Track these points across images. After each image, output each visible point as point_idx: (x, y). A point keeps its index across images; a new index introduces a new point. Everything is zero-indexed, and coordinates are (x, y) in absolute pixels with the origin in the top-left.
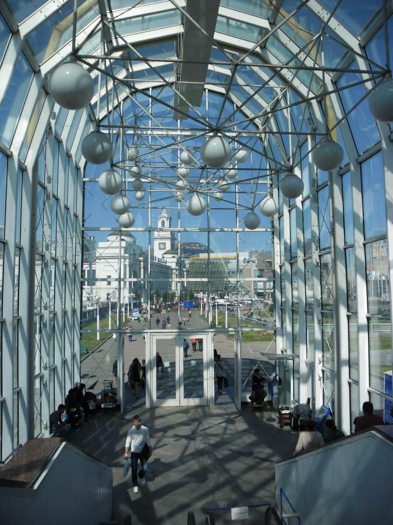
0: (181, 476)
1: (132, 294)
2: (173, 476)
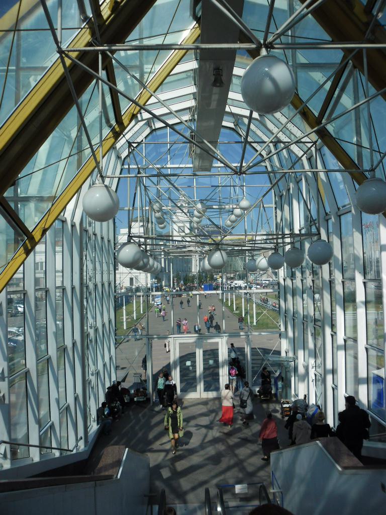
0: (201, 459)
1: (154, 280)
2: (195, 459)
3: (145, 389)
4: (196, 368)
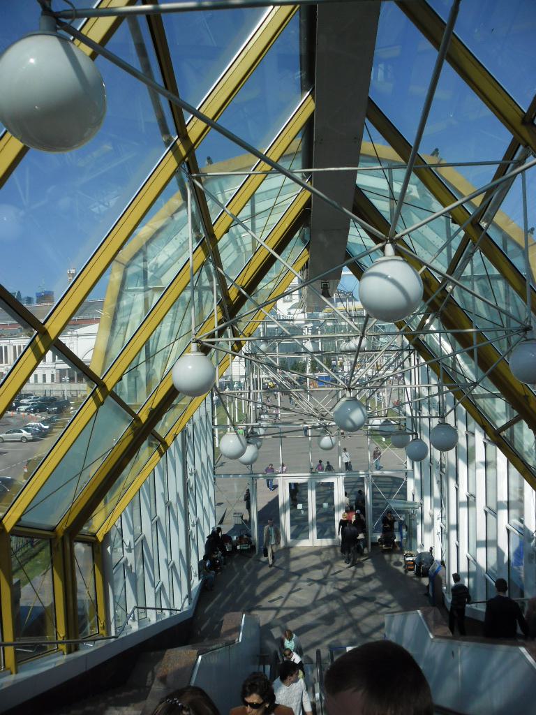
3: (249, 536)
4: (307, 505)
